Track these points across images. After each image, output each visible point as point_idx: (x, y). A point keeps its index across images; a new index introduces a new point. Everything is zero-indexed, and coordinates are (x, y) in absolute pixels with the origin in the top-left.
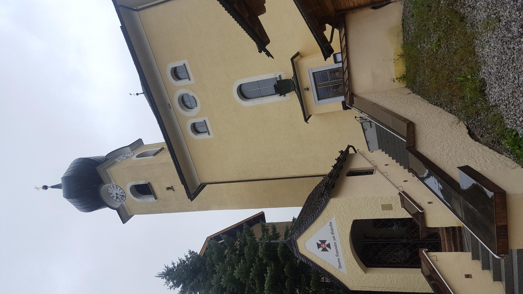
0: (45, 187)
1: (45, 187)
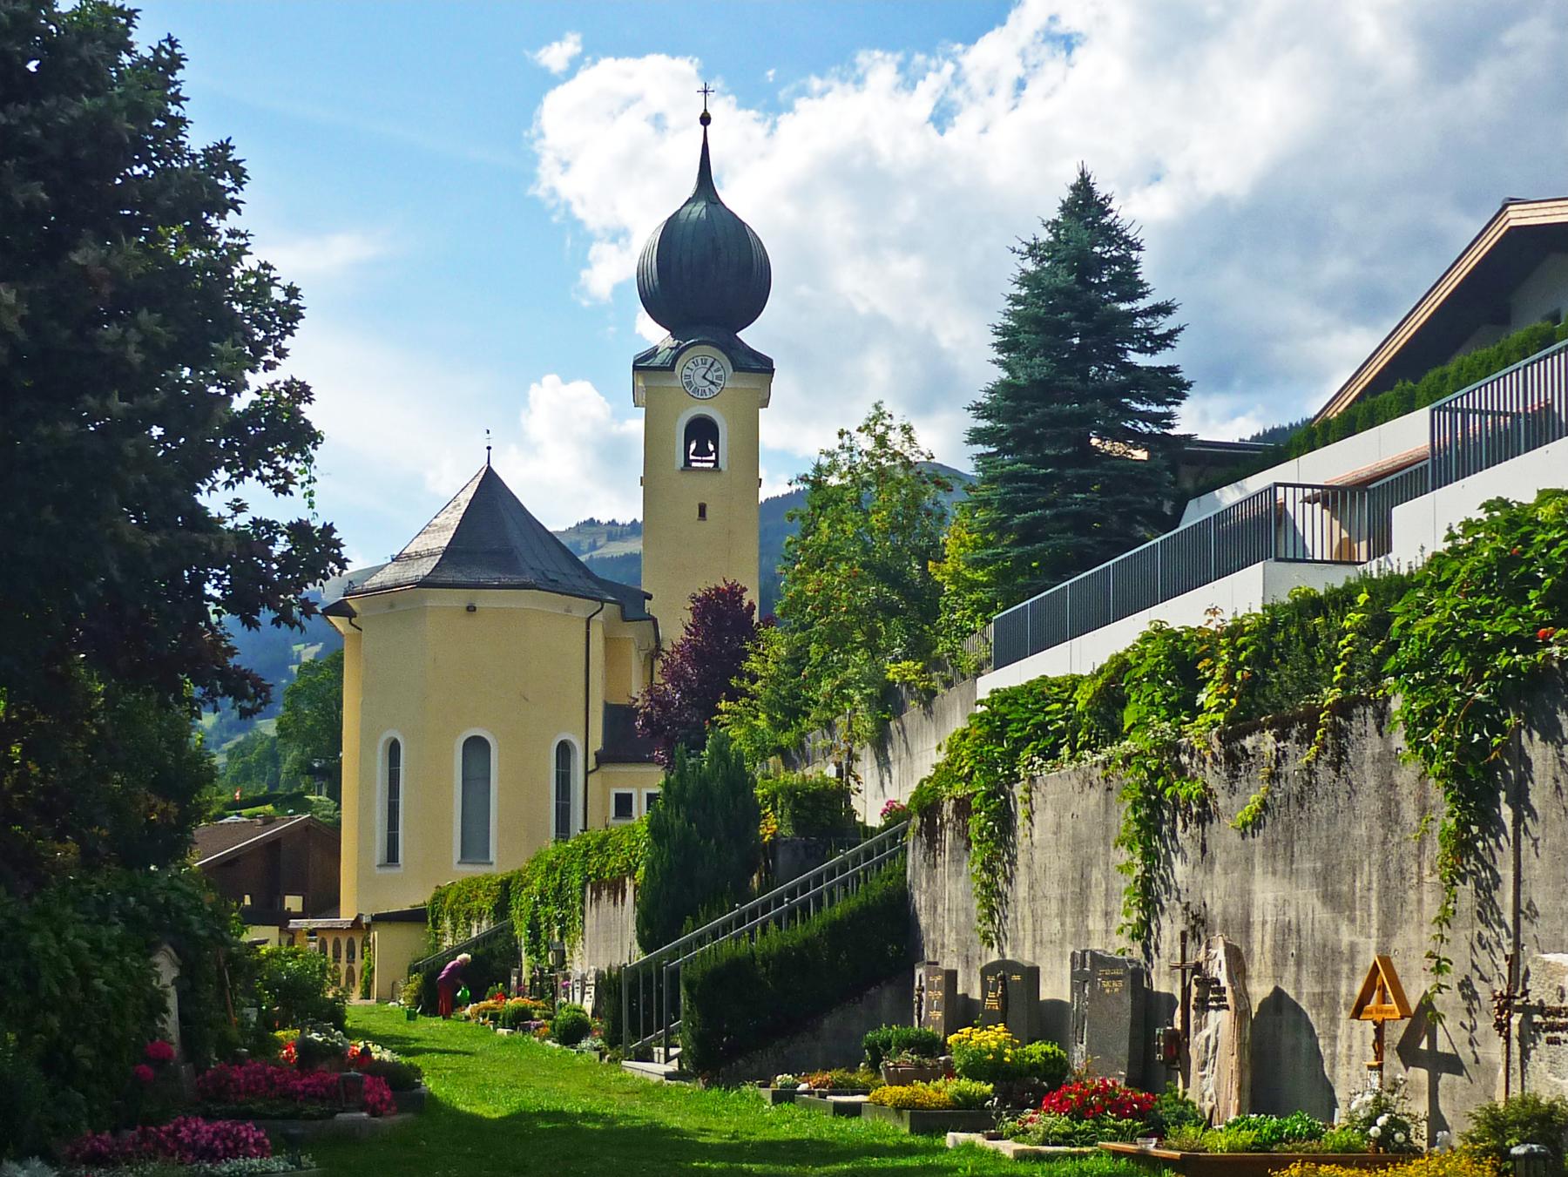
0: (705, 120)
1: (705, 120)
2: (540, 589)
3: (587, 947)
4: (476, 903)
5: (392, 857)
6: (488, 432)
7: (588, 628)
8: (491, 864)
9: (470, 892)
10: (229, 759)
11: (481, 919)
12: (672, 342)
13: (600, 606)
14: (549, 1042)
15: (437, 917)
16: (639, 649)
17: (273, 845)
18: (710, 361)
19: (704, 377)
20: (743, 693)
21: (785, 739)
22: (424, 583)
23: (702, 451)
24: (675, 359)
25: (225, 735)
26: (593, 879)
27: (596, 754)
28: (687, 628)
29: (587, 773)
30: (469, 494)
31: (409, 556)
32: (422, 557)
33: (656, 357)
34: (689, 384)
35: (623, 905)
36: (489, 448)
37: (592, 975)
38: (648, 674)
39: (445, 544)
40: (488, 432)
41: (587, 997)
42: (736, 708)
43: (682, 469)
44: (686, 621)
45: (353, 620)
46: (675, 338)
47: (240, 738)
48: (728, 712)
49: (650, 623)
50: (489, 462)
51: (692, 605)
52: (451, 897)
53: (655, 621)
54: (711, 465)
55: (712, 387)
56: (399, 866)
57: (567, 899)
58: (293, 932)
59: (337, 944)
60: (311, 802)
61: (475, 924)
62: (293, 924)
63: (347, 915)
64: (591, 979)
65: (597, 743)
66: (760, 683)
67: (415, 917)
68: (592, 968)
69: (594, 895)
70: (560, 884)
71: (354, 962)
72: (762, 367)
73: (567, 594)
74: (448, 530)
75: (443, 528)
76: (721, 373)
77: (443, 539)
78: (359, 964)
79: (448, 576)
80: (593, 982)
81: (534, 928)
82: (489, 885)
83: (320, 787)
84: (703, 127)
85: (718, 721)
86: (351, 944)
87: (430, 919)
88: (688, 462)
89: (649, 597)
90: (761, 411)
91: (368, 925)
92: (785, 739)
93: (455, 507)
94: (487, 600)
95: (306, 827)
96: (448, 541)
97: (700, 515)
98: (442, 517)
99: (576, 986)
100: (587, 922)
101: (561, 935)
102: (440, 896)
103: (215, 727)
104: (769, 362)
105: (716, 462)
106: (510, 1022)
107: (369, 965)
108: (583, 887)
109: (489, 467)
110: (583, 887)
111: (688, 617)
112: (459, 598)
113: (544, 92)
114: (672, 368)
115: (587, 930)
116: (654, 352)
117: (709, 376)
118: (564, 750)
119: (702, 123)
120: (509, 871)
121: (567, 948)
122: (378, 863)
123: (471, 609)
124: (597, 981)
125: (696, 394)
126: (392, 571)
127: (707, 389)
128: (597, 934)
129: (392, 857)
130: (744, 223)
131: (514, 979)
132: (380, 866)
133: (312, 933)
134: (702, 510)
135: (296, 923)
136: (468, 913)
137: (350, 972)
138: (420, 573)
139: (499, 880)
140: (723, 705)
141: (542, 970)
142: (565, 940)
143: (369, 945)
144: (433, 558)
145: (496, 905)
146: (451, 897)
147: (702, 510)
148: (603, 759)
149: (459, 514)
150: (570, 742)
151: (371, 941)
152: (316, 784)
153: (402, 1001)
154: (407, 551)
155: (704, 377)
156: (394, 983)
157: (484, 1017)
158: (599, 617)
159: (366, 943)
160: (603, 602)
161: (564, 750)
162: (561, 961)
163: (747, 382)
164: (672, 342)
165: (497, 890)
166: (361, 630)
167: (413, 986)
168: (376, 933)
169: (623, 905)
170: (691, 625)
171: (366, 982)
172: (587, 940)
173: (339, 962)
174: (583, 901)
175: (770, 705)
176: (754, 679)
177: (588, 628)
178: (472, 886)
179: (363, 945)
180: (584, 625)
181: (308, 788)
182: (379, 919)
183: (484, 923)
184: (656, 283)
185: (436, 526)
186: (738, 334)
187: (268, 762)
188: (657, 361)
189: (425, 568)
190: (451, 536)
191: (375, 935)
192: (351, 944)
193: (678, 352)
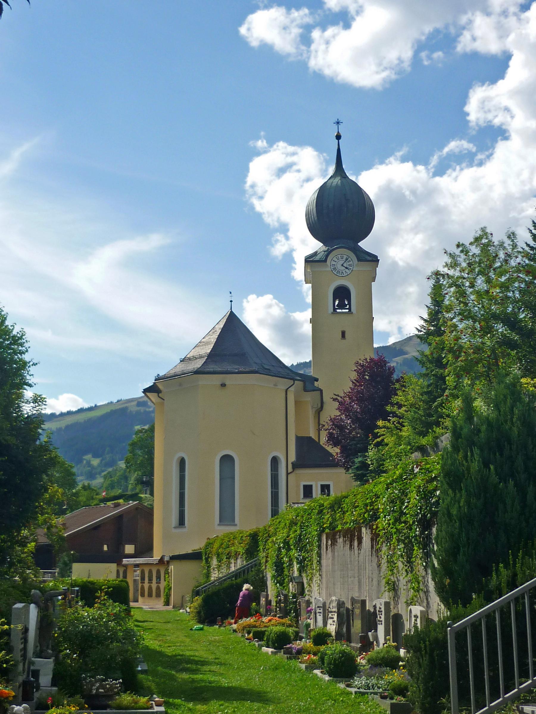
0: (338, 137)
1: (338, 137)
2: (260, 374)
3: (324, 580)
4: (233, 548)
5: (181, 522)
6: (231, 293)
7: (286, 394)
8: (236, 525)
9: (229, 541)
10: (105, 479)
11: (237, 559)
12: (326, 249)
13: (292, 383)
14: (317, 672)
15: (209, 557)
16: (312, 408)
17: (119, 518)
18: (345, 257)
19: (342, 265)
20: (395, 415)
21: (424, 441)
22: (197, 372)
23: (342, 306)
24: (327, 256)
25: (103, 469)
26: (327, 531)
27: (292, 463)
28: (353, 382)
29: (288, 474)
30: (221, 325)
31: (189, 359)
32: (196, 359)
33: (317, 256)
34: (335, 269)
35: (359, 549)
36: (231, 301)
37: (335, 604)
38: (317, 419)
39: (209, 352)
40: (231, 293)
41: (330, 621)
42: (388, 424)
43: (332, 313)
44: (353, 378)
45: (160, 395)
46: (326, 246)
47: (110, 469)
48: (384, 427)
49: (319, 392)
50: (231, 309)
51: (356, 368)
52: (216, 546)
53: (321, 391)
54: (347, 310)
55: (347, 270)
56: (185, 527)
57: (306, 545)
58: (126, 566)
59: (150, 572)
60: (141, 498)
61: (232, 561)
62: (125, 561)
63: (156, 557)
64: (333, 607)
65: (292, 458)
66: (404, 408)
67: (195, 556)
68: (334, 598)
69: (330, 542)
70: (300, 535)
71: (160, 583)
72: (374, 260)
73: (275, 376)
74: (210, 344)
75: (207, 343)
76: (351, 263)
77: (208, 349)
78: (163, 584)
79: (212, 367)
80: (335, 610)
81: (279, 567)
82: (242, 537)
83: (146, 490)
84: (337, 141)
85: (378, 433)
86: (158, 572)
87: (204, 558)
88: (335, 310)
89: (317, 380)
90: (373, 283)
91: (168, 562)
92: (424, 441)
93: (214, 332)
94: (230, 380)
95: (136, 509)
96: (210, 349)
97: (342, 337)
98: (207, 338)
99: (318, 611)
100: (324, 562)
101: (300, 571)
102: (209, 545)
103: (99, 465)
104: (376, 257)
105: (350, 309)
106: (273, 644)
107: (169, 586)
108: (320, 536)
109: (232, 312)
110: (320, 536)
111: (354, 376)
112: (217, 379)
113: (250, 160)
114: (325, 261)
115: (324, 569)
116: (315, 254)
117: (345, 265)
118: (275, 461)
119: (337, 139)
120: (255, 527)
121: (305, 581)
122: (173, 526)
123: (223, 385)
124: (338, 609)
125: (339, 274)
126: (181, 367)
127: (344, 271)
128: (334, 571)
129: (181, 522)
130: (361, 188)
131: (263, 601)
132: (175, 528)
133: (137, 566)
134: (343, 334)
135: (128, 561)
136: (228, 554)
137: (158, 588)
138: (195, 367)
139: (248, 534)
140: (380, 423)
141: (286, 596)
142: (304, 575)
143: (168, 573)
144: (202, 359)
145: (247, 549)
146: (216, 546)
147: (343, 334)
148: (296, 466)
149: (216, 336)
150: (278, 457)
151: (170, 571)
152: (144, 489)
153: (188, 610)
154: (188, 356)
155: (342, 265)
156: (183, 597)
157: (249, 633)
158: (292, 389)
159: (167, 572)
160: (294, 380)
161: (275, 461)
162: (302, 592)
163: (365, 267)
164: (326, 249)
165: (248, 540)
166: (164, 400)
167: (196, 604)
168: (172, 567)
169: (359, 549)
170: (355, 380)
171: (167, 595)
172: (324, 576)
173: (152, 583)
174: (319, 547)
175: (413, 421)
176: (400, 406)
177: (286, 394)
178: (231, 538)
179: (165, 574)
180: (285, 392)
181: (140, 491)
182: (174, 558)
183: (239, 561)
184: (316, 218)
185: (204, 342)
186: (359, 244)
187: (122, 481)
188: (317, 258)
189: (198, 364)
190: (212, 347)
191: (172, 567)
192: (158, 572)
193: (328, 253)
